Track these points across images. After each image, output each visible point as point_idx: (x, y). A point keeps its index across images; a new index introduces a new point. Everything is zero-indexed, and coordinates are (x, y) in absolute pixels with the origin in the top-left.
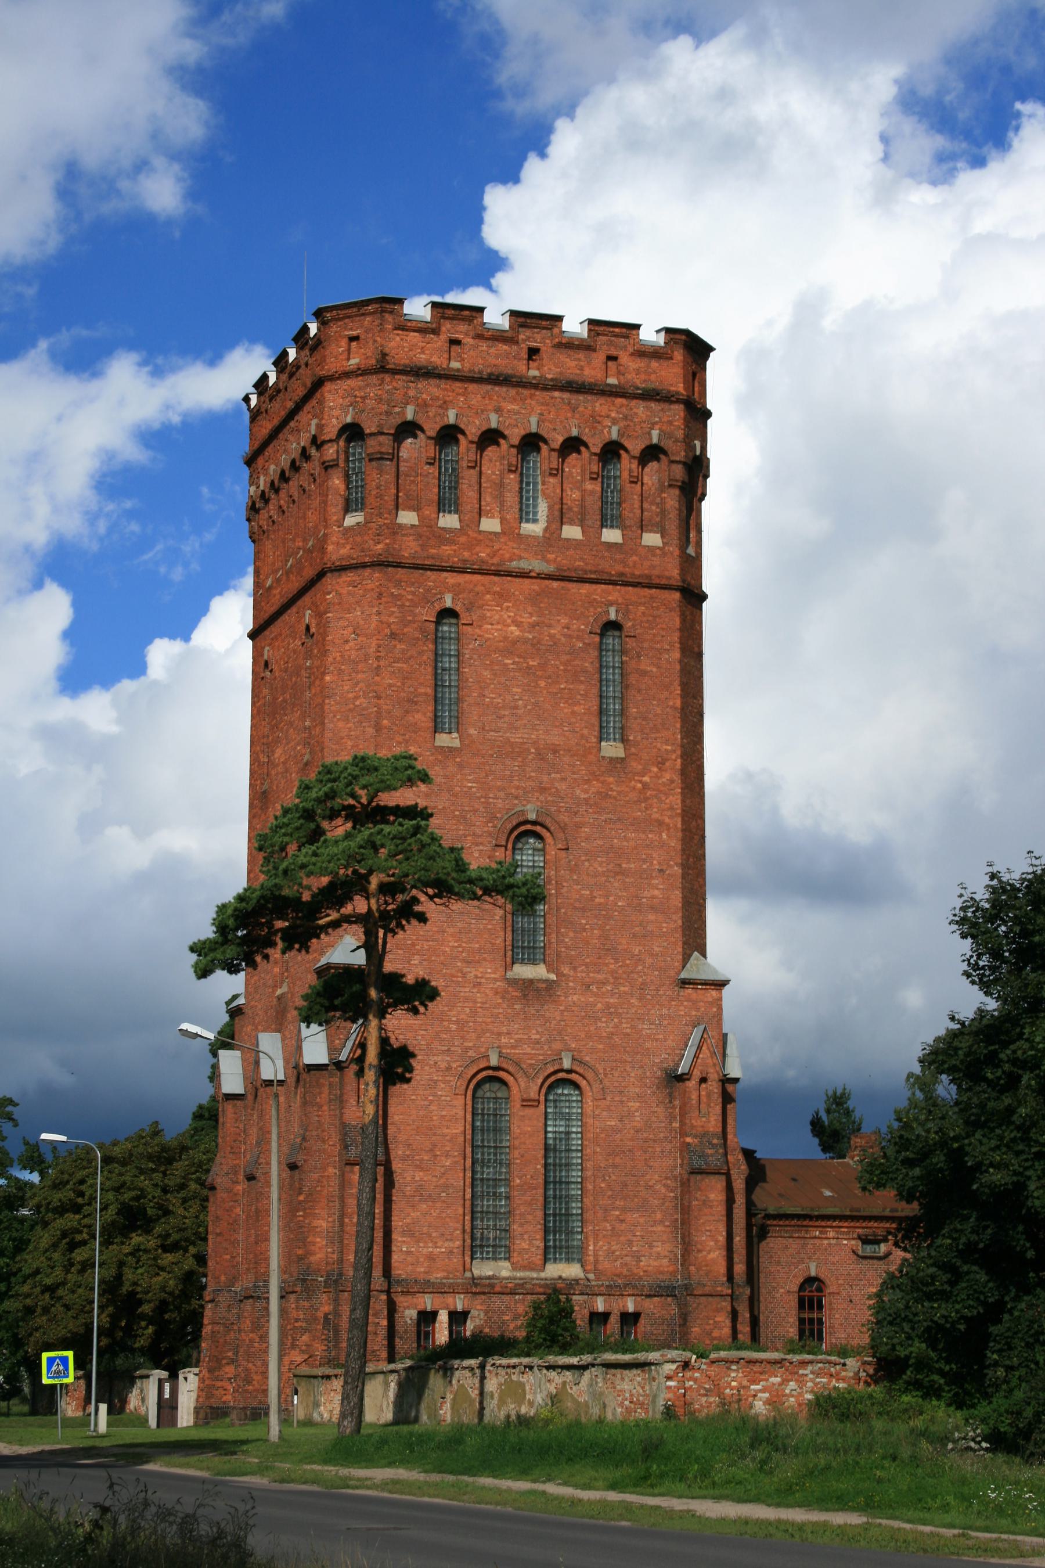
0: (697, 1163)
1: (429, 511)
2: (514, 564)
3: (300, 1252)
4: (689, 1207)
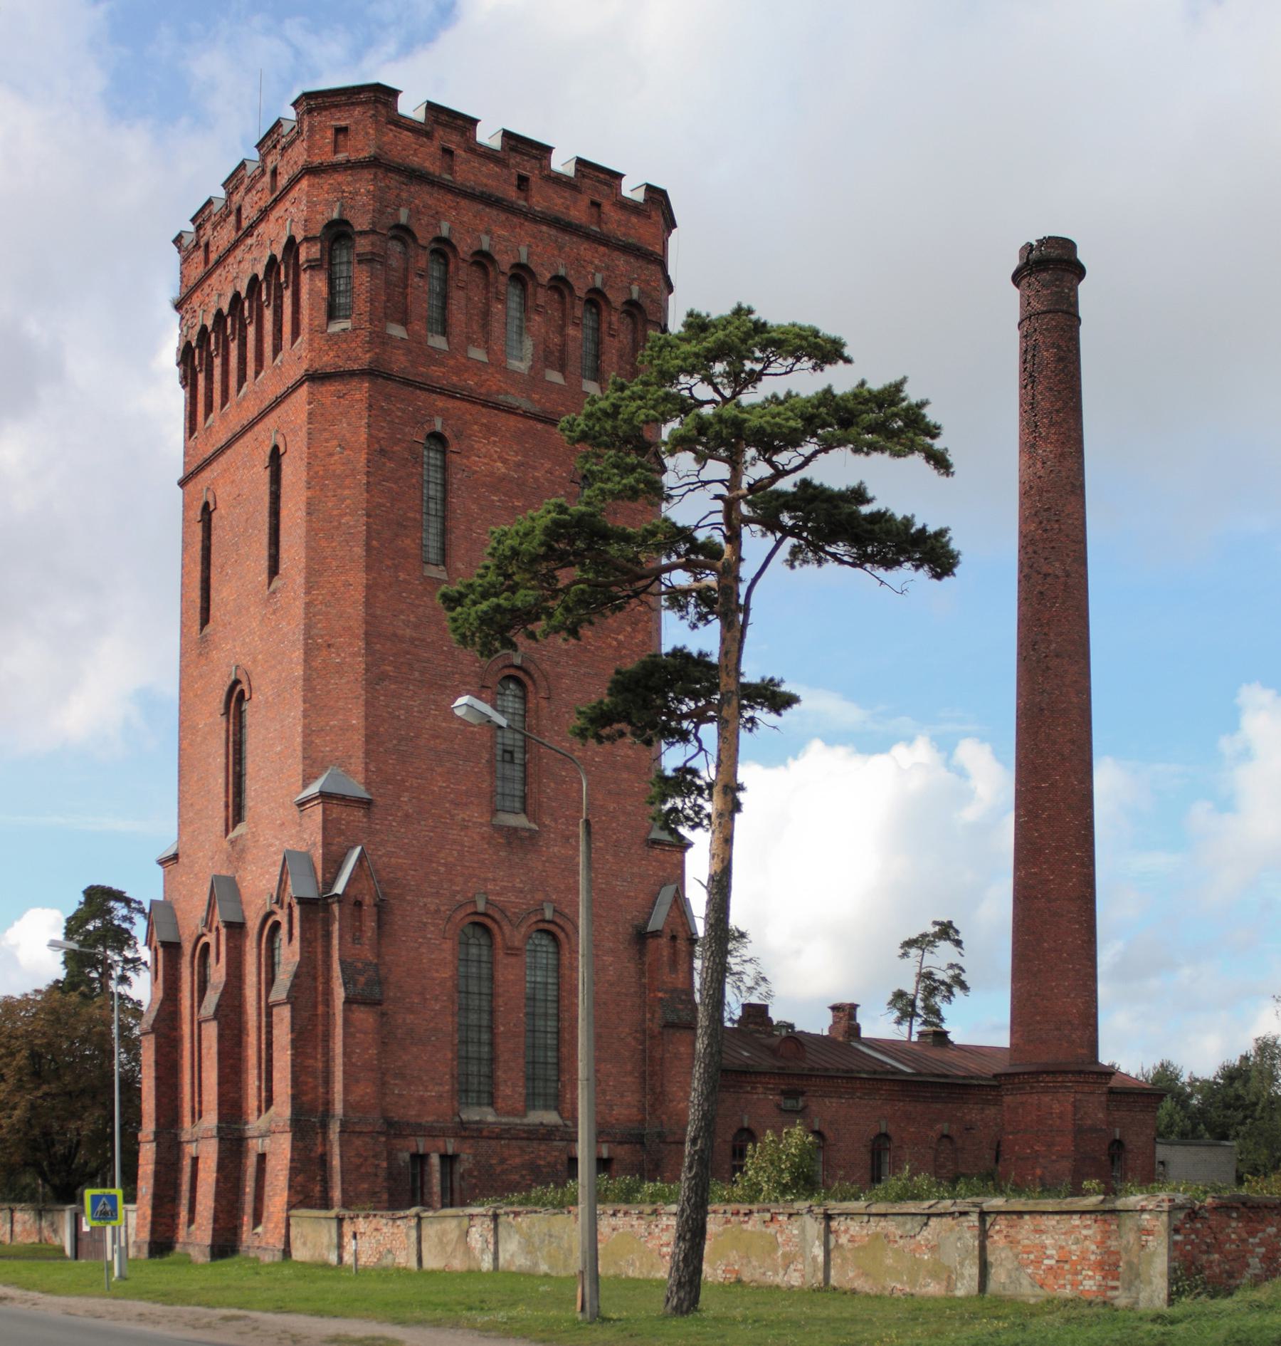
0: (672, 1017)
2: (501, 397)
4: (662, 1059)
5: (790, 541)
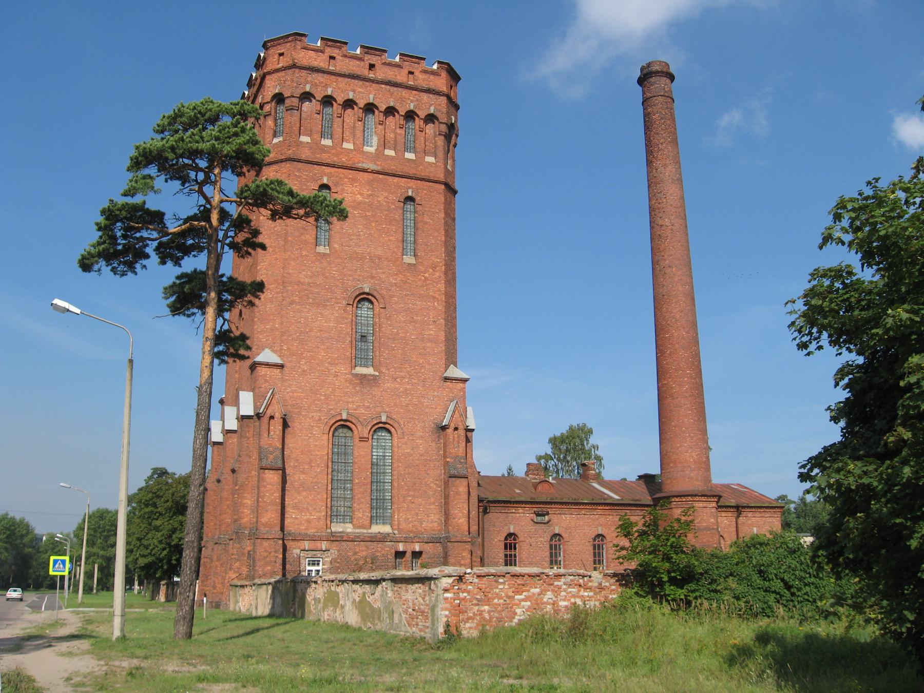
0: (453, 472)
1: (317, 136)
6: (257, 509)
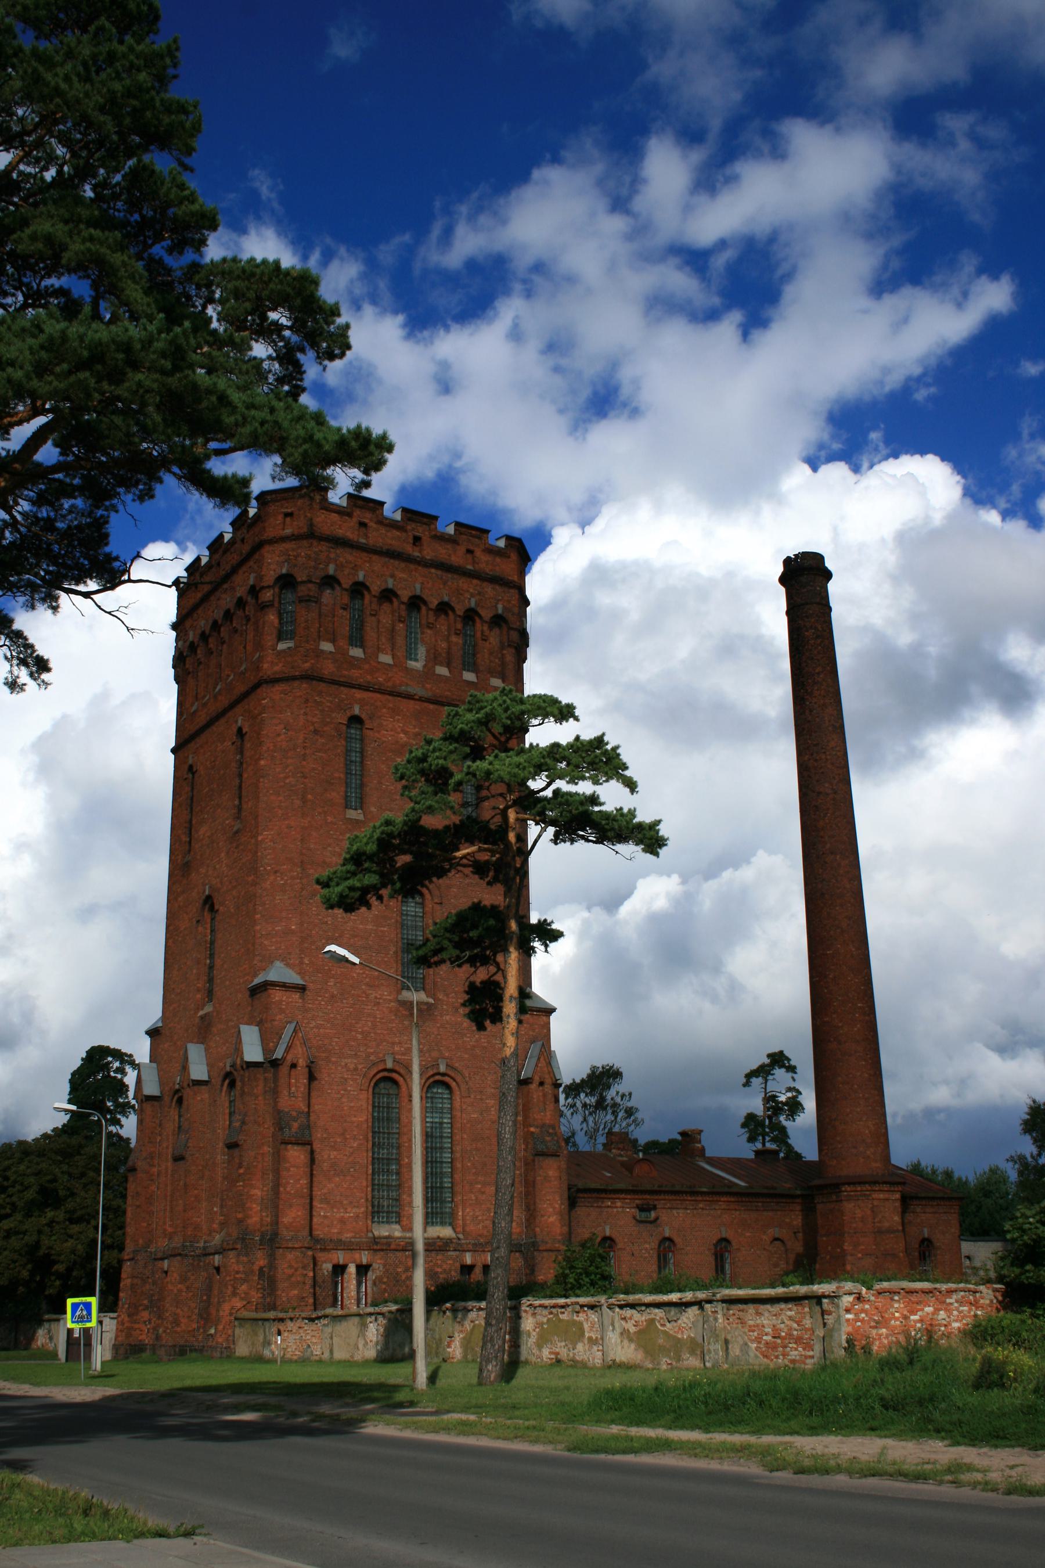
0: (541, 1147)
1: (342, 643)
3: (240, 1216)
4: (534, 1182)
5: (551, 830)
6: (275, 1201)
